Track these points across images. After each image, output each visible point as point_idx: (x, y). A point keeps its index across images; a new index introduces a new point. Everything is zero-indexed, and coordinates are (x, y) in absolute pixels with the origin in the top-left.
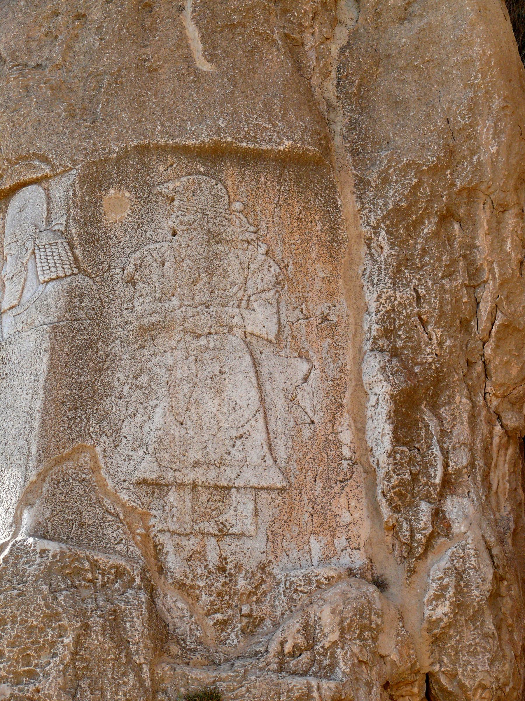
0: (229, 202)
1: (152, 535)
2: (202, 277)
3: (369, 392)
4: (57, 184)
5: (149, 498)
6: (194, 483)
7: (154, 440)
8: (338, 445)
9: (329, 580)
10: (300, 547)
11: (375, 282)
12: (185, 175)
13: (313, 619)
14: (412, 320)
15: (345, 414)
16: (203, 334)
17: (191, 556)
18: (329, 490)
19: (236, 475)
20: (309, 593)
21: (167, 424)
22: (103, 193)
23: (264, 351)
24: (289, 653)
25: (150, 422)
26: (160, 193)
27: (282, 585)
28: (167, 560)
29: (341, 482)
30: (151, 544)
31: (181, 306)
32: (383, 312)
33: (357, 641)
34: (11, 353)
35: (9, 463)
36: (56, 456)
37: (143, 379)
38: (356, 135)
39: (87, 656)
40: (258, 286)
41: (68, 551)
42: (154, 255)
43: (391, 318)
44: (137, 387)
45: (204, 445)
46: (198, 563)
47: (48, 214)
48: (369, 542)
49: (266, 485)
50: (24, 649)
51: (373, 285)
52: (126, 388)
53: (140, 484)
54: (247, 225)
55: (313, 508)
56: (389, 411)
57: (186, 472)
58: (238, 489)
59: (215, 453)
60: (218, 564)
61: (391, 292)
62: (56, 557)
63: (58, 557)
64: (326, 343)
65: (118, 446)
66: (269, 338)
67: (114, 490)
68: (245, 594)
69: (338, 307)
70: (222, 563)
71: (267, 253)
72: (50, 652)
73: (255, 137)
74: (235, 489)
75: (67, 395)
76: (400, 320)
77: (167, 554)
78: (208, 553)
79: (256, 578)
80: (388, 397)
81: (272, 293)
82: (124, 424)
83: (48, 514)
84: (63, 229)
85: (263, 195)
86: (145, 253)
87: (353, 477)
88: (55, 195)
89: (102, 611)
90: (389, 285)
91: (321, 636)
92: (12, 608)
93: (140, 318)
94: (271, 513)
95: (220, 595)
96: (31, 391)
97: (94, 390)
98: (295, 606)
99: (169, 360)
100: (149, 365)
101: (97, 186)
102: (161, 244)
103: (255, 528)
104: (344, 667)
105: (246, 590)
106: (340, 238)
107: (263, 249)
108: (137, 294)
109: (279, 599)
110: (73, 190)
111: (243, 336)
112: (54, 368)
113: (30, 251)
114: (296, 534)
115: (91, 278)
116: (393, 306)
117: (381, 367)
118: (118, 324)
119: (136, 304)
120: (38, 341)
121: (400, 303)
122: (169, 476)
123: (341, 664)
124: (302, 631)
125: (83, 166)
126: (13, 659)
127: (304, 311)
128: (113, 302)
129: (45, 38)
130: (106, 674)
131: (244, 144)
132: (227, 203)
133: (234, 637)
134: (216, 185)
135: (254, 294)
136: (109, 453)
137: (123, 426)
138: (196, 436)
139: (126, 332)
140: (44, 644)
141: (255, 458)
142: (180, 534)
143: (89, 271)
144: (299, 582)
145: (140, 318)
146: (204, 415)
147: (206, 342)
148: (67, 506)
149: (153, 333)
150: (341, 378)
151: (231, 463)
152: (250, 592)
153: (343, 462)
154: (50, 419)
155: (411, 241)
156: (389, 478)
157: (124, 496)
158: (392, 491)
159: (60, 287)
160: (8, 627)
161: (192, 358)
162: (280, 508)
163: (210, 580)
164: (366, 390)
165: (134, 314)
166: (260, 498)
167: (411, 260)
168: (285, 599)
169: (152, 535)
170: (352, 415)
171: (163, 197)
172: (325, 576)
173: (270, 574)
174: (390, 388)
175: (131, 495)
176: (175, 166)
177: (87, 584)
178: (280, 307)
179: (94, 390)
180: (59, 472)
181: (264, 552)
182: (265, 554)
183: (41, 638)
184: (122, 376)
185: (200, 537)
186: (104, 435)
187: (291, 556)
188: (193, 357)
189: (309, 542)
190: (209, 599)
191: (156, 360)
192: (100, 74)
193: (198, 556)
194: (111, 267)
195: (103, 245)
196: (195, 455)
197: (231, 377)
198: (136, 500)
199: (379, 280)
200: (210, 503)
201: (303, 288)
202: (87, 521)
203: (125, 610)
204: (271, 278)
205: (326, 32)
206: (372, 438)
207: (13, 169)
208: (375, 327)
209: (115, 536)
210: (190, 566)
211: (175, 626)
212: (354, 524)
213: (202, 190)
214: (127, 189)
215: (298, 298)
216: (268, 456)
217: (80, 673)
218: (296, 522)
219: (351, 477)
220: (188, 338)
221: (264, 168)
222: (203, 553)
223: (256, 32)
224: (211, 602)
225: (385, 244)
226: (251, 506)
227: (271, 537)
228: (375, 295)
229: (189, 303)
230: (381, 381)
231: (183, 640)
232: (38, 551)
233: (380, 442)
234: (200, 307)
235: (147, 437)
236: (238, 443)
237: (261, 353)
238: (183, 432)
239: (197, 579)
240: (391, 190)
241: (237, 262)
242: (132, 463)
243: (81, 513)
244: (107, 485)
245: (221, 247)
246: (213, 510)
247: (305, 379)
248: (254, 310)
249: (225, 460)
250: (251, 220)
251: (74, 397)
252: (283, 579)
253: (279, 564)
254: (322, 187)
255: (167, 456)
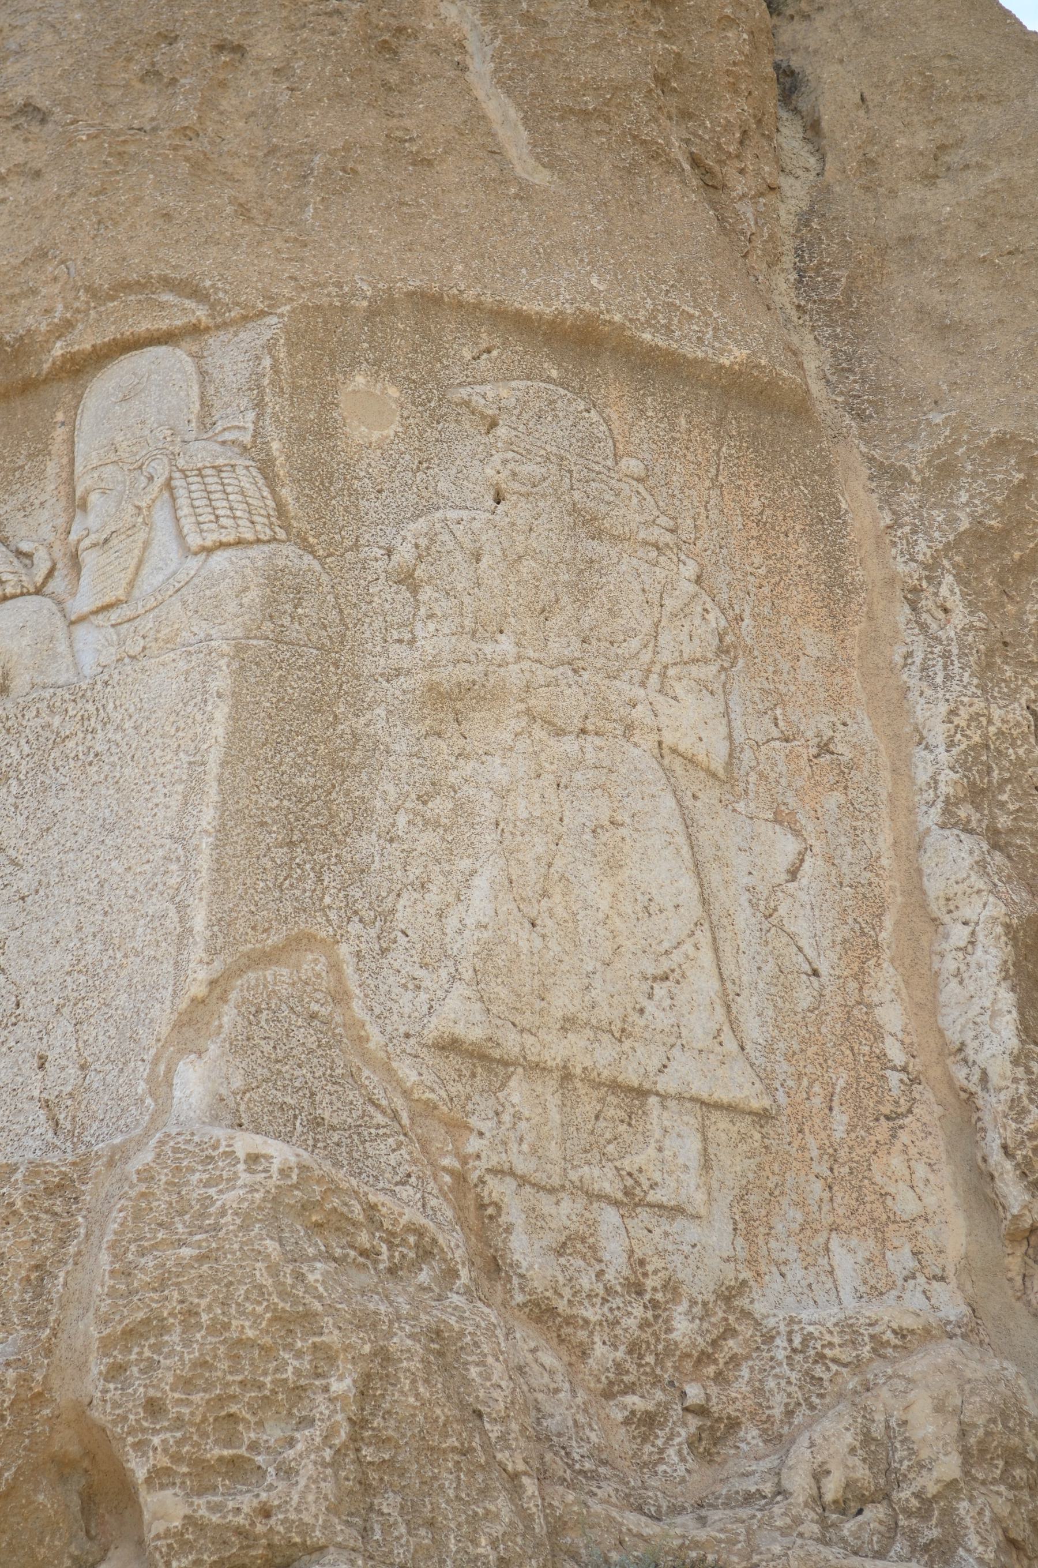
0: (615, 455)
1: (474, 1177)
2: (562, 603)
3: (946, 919)
4: (223, 344)
5: (464, 1086)
6: (565, 1067)
7: (475, 949)
8: (877, 1033)
9: (904, 1337)
10: (809, 1259)
11: (939, 680)
12: (518, 378)
13: (882, 1426)
14: (1030, 772)
15: (885, 965)
16: (569, 729)
17: (565, 1243)
18: (862, 1133)
19: (659, 1066)
20: (857, 1365)
21: (501, 916)
22: (340, 377)
23: (699, 794)
24: (835, 1502)
25: (461, 907)
26: (467, 403)
27: (781, 1342)
28: (511, 1245)
29: (888, 1118)
30: (470, 1201)
31: (519, 658)
32: (963, 747)
33: (1002, 1488)
34: (111, 706)
35: (119, 955)
36: (250, 946)
37: (440, 806)
38: (855, 382)
39: (390, 1433)
40: (683, 647)
41: (315, 1167)
42: (458, 534)
43: (982, 763)
44: (426, 822)
45: (586, 981)
46: (581, 1263)
47: (202, 405)
48: (966, 1266)
49: (726, 1100)
50: (220, 1398)
51: (935, 687)
52: (402, 820)
53: (443, 1048)
54: (656, 513)
55: (831, 1170)
56: (1006, 962)
57: (548, 1038)
58: (663, 1097)
59: (611, 1006)
60: (626, 1272)
61: (979, 705)
62: (289, 1176)
63: (295, 1177)
64: (833, 801)
65: (387, 950)
66: (713, 767)
67: (382, 1054)
68: (689, 1355)
69: (853, 728)
70: (635, 1272)
71: (698, 580)
72: (290, 1414)
73: (667, 327)
74: (658, 1099)
75: (272, 809)
76: (1001, 769)
77: (509, 1229)
78: (603, 1243)
79: (713, 1320)
80: (999, 930)
81: (714, 669)
82: (402, 902)
83: (238, 1082)
84: (247, 438)
85: (685, 456)
86: (438, 526)
87: (915, 1111)
88: (221, 367)
89: (413, 1326)
90: (974, 690)
91: (910, 1467)
92: (182, 1292)
93: (430, 666)
94: (738, 1169)
95: (633, 1349)
96: (180, 788)
97: (329, 809)
98: (821, 1396)
99: (498, 771)
100: (453, 777)
101: (327, 359)
102: (473, 514)
103: (705, 1197)
104: (981, 1549)
105: (695, 1345)
106: (848, 580)
107: (690, 570)
108: (422, 611)
109: (776, 1376)
110: (273, 357)
111: (656, 751)
112: (241, 739)
113: (159, 481)
114: (796, 1227)
115: (315, 557)
116: (985, 736)
117: (977, 863)
118: (379, 671)
119: (419, 632)
120: (195, 676)
121: (1000, 733)
122: (511, 1042)
123: (973, 1541)
124: (860, 1452)
125: (293, 311)
126: (192, 1424)
127: (781, 723)
128: (367, 620)
129: (139, 86)
130: (441, 1487)
131: (647, 336)
132: (611, 455)
133: (676, 1459)
134: (588, 411)
135: (675, 664)
136: (368, 963)
137: (399, 907)
138: (566, 958)
139: (398, 693)
140: (274, 1392)
141: (699, 1033)
142: (538, 1187)
143: (311, 540)
144: (828, 1337)
145: (430, 666)
146: (582, 913)
147: (576, 747)
148: (279, 1072)
149: (459, 705)
150: (870, 884)
151: (647, 1035)
152: (703, 1352)
153: (888, 1073)
154: (234, 856)
155: (1009, 607)
156: (1018, 1114)
157: (408, 1073)
158: (1028, 1144)
159: (247, 562)
160: (174, 1338)
161: (548, 779)
162: (758, 1159)
163: (611, 1309)
164: (936, 914)
165: (417, 655)
166: (713, 1128)
167: (1014, 647)
168: (794, 1376)
169: (474, 1177)
170: (900, 970)
171: (473, 413)
172: (895, 1325)
173: (746, 1314)
174: (1004, 909)
175: (424, 1071)
176: (495, 353)
177: (361, 1260)
178: (731, 704)
179: (329, 809)
180: (258, 986)
181: (728, 1260)
182: (732, 1264)
183: (265, 1373)
184: (392, 790)
185: (582, 1200)
186: (356, 919)
187: (789, 1276)
188: (551, 777)
189: (827, 1250)
190: (612, 1356)
191: (468, 768)
192: (300, 151)
193: (579, 1246)
194: (362, 542)
195: (342, 490)
196: (567, 1002)
197: (635, 836)
198: (436, 1086)
199: (948, 677)
200: (601, 1123)
201: (775, 672)
202: (326, 1116)
203: (461, 1334)
204: (709, 637)
205: (770, 174)
206: (962, 1020)
207: (102, 309)
208: (947, 776)
209: (393, 1163)
210: (564, 1269)
211: (539, 1410)
212: (927, 1220)
213: (556, 416)
214: (393, 380)
215: (768, 692)
216: (727, 1036)
217: (373, 1475)
218: (794, 1197)
219: (910, 1111)
220: (539, 732)
221: (685, 399)
222: (591, 1240)
223: (634, 137)
224: (618, 1365)
225: (955, 603)
226: (694, 1144)
227: (742, 1225)
228: (943, 709)
229: (536, 655)
230: (979, 892)
231: (564, 1448)
232: (241, 1155)
233: (988, 1030)
234: (561, 669)
235: (454, 941)
236: (660, 991)
237: (695, 797)
238: (538, 943)
239: (581, 1303)
240: (962, 493)
241: (638, 587)
242: (423, 996)
243: (313, 1094)
244: (368, 1040)
245: (601, 548)
246: (609, 1142)
247: (793, 874)
248: (675, 698)
249: (633, 1026)
250: (661, 504)
251: (286, 816)
252: (783, 1328)
253: (767, 1291)
254: (804, 465)
255: (503, 992)
